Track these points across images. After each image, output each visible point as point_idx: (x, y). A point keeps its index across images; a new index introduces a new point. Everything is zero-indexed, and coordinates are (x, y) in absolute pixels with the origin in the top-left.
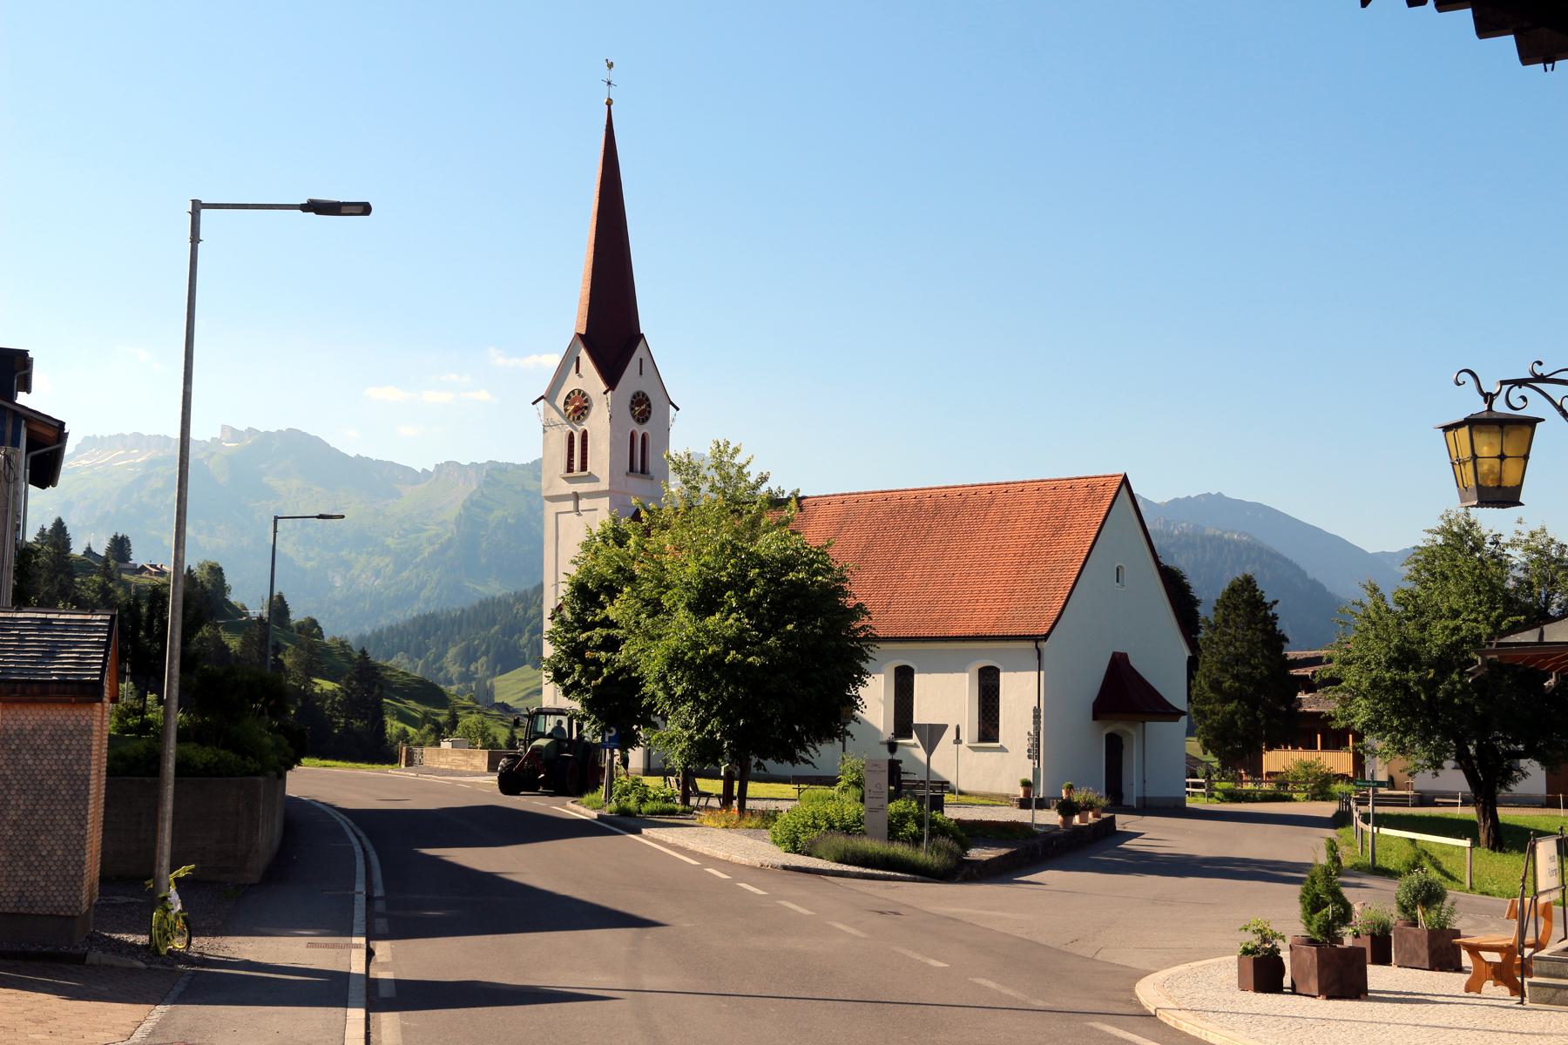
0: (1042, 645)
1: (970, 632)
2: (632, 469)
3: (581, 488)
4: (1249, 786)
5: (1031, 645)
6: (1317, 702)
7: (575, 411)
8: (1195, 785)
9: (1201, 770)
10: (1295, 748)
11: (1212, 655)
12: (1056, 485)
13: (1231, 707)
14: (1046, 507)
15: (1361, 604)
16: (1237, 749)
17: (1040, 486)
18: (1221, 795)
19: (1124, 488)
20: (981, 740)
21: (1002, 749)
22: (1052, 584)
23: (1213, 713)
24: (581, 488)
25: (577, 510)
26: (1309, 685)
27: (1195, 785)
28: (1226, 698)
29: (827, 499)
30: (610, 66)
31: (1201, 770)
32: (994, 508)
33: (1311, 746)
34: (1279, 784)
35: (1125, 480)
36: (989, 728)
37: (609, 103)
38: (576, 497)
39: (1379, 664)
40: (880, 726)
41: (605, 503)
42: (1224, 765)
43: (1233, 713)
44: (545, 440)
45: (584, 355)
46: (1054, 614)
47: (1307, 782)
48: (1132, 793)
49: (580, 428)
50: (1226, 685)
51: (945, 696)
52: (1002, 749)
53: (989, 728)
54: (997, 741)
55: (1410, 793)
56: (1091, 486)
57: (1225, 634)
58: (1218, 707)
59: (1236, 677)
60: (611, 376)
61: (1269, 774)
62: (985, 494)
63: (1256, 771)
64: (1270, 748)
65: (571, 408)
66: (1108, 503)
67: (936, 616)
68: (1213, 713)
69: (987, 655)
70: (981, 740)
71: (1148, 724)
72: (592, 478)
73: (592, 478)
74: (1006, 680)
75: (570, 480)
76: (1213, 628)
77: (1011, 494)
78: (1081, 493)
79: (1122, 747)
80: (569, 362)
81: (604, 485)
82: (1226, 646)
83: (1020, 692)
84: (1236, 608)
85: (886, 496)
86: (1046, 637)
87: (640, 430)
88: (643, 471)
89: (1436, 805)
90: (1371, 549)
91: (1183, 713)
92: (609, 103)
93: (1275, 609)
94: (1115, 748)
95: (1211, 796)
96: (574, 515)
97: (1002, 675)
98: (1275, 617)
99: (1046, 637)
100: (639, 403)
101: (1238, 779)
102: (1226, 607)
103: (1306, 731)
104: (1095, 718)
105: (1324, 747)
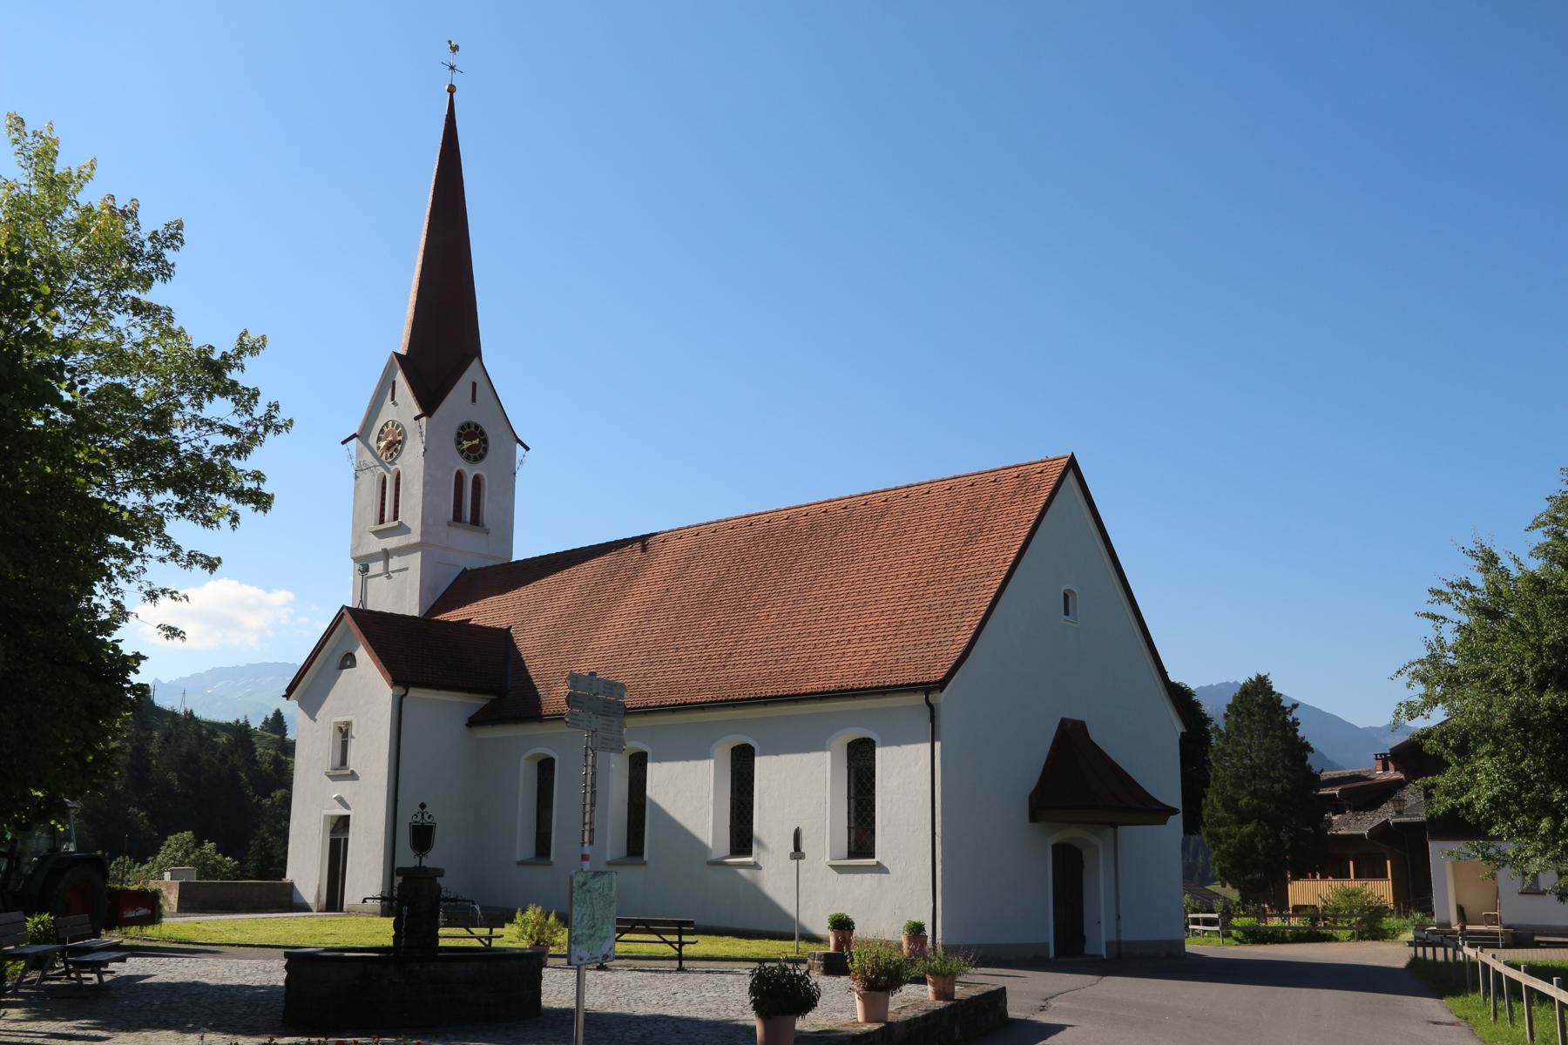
0: (938, 698)
1: (831, 685)
2: (458, 516)
3: (392, 542)
4: (1275, 922)
5: (920, 699)
6: (1347, 824)
7: (388, 447)
8: (1207, 922)
9: (1218, 905)
10: (1324, 877)
11: (1225, 768)
12: (973, 482)
13: (1249, 828)
14: (959, 509)
15: (1467, 586)
16: (1262, 882)
17: (952, 485)
18: (1240, 935)
19: (1071, 476)
20: (851, 855)
21: (880, 869)
22: (958, 609)
23: (1229, 836)
24: (392, 542)
25: (386, 571)
26: (1337, 806)
27: (1207, 922)
28: (1243, 817)
29: (678, 533)
30: (455, 49)
31: (1218, 905)
32: (888, 518)
33: (1343, 875)
34: (1314, 920)
35: (1072, 464)
36: (861, 840)
37: (452, 90)
38: (386, 555)
39: (1521, 679)
40: (707, 837)
41: (415, 560)
42: (1245, 898)
43: (1252, 836)
44: (357, 488)
45: (400, 378)
46: (955, 651)
47: (1351, 915)
48: (1099, 939)
49: (392, 468)
50: (1243, 802)
51: (798, 788)
52: (880, 869)
53: (861, 840)
54: (872, 855)
55: (1497, 928)
56: (1023, 476)
57: (1239, 744)
58: (1234, 829)
59: (1254, 794)
60: (429, 401)
61: (1297, 909)
62: (878, 504)
63: (1280, 903)
64: (1296, 877)
65: (383, 444)
66: (1046, 493)
67: (788, 668)
68: (1229, 836)
69: (854, 722)
70: (851, 855)
71: (1122, 830)
72: (402, 529)
73: (402, 529)
74: (887, 760)
75: (379, 534)
76: (1225, 737)
77: (913, 498)
78: (1009, 485)
79: (1082, 866)
80: (386, 387)
81: (415, 537)
82: (1241, 759)
83: (906, 775)
84: (1250, 714)
85: (750, 520)
86: (941, 685)
87: (470, 471)
88: (476, 520)
89: (1537, 945)
90: (1361, 725)
91: (1174, 811)
92: (452, 90)
93: (1295, 713)
94: (1069, 871)
95: (1228, 935)
96: (383, 578)
97: (878, 751)
98: (1296, 723)
99: (941, 685)
100: (470, 437)
101: (1262, 915)
102: (1239, 714)
103: (1329, 858)
104: (1034, 817)
105: (1357, 876)
